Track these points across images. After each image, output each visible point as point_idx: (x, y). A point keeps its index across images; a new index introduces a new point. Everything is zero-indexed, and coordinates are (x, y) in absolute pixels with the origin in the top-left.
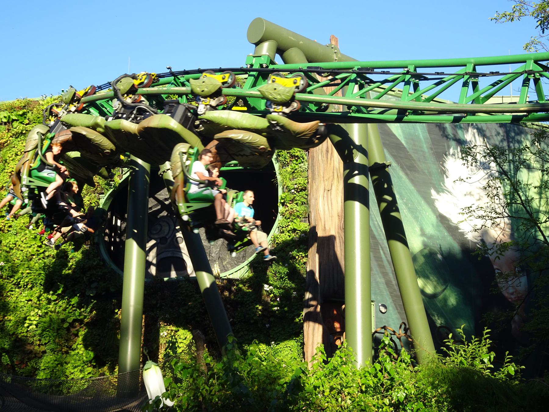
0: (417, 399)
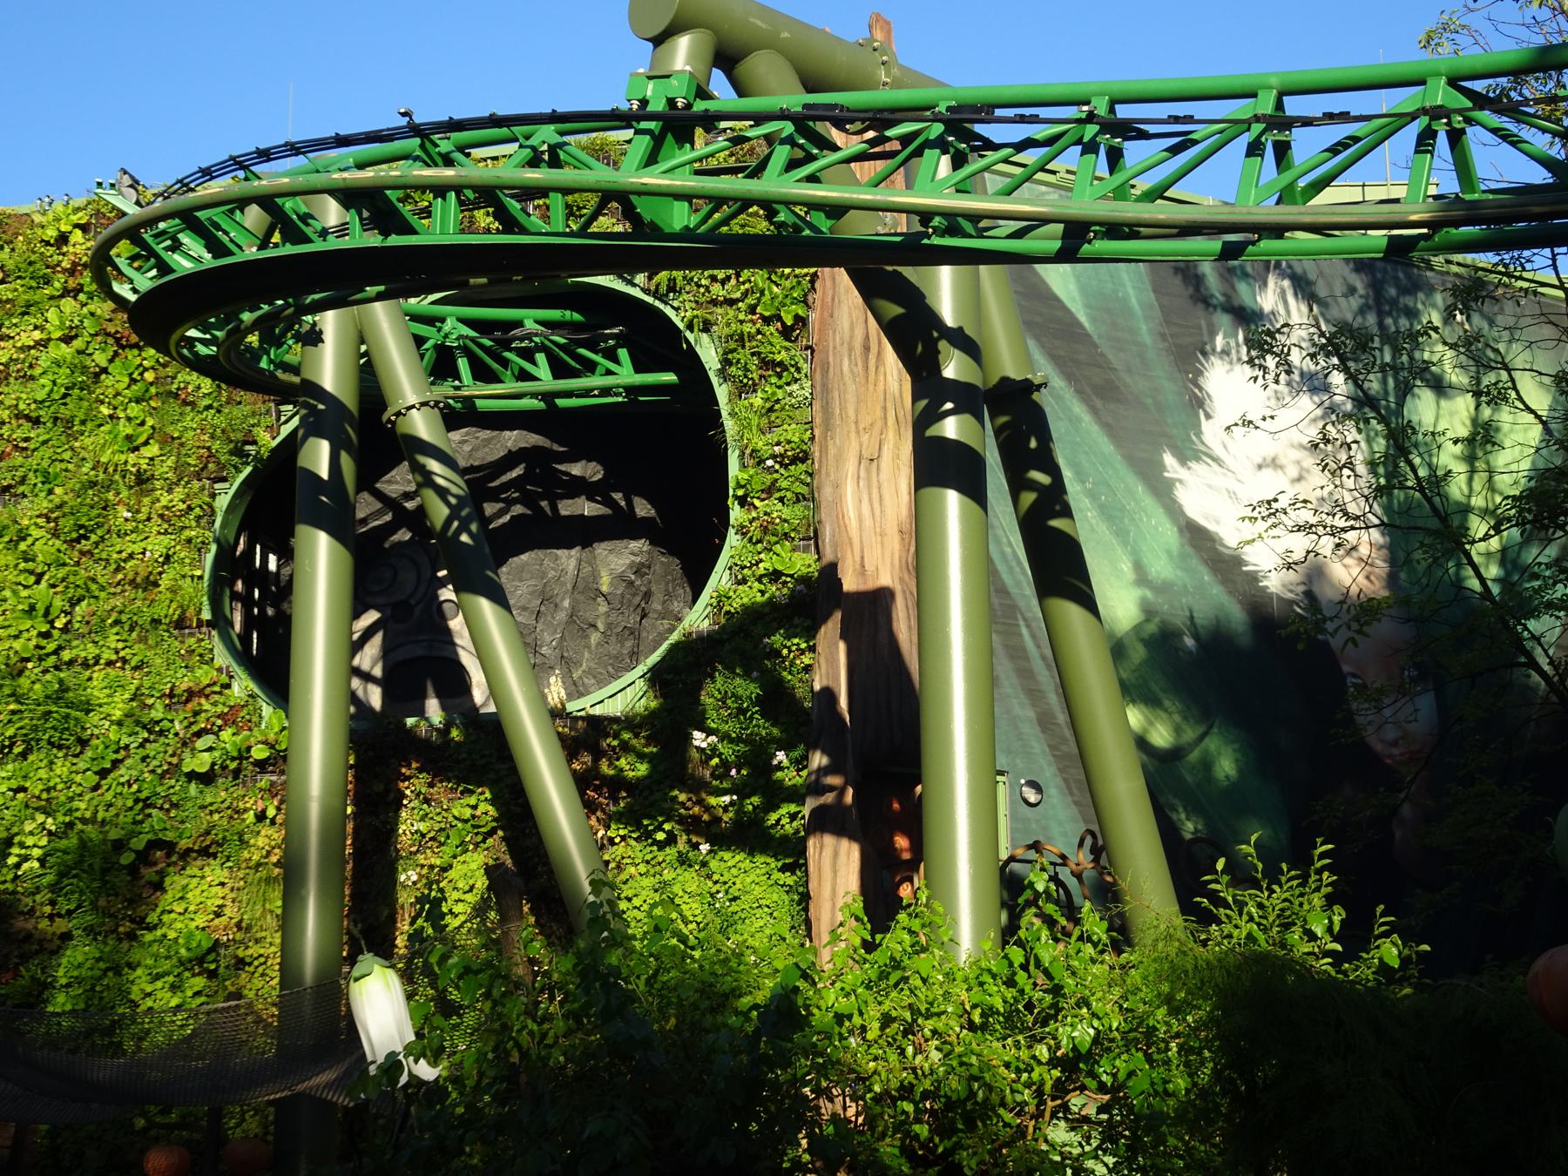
0: (1129, 1044)
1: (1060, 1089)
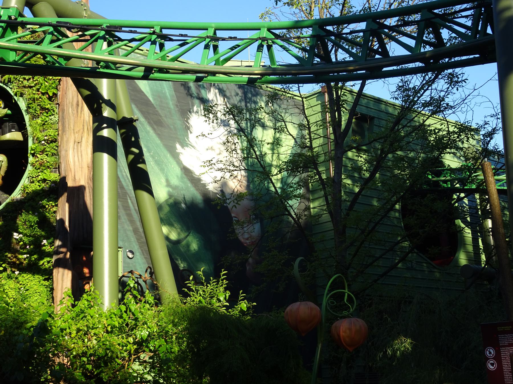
0: (160, 336)
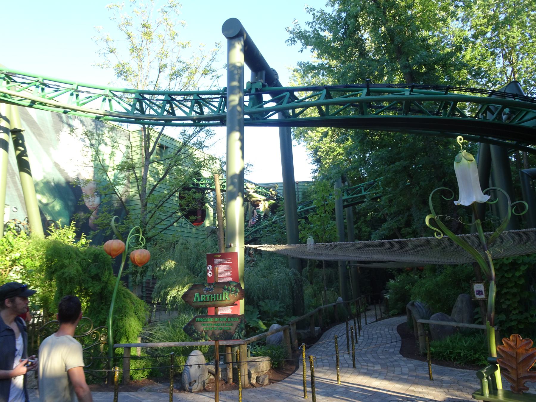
0: (27, 257)
1: (12, 266)
